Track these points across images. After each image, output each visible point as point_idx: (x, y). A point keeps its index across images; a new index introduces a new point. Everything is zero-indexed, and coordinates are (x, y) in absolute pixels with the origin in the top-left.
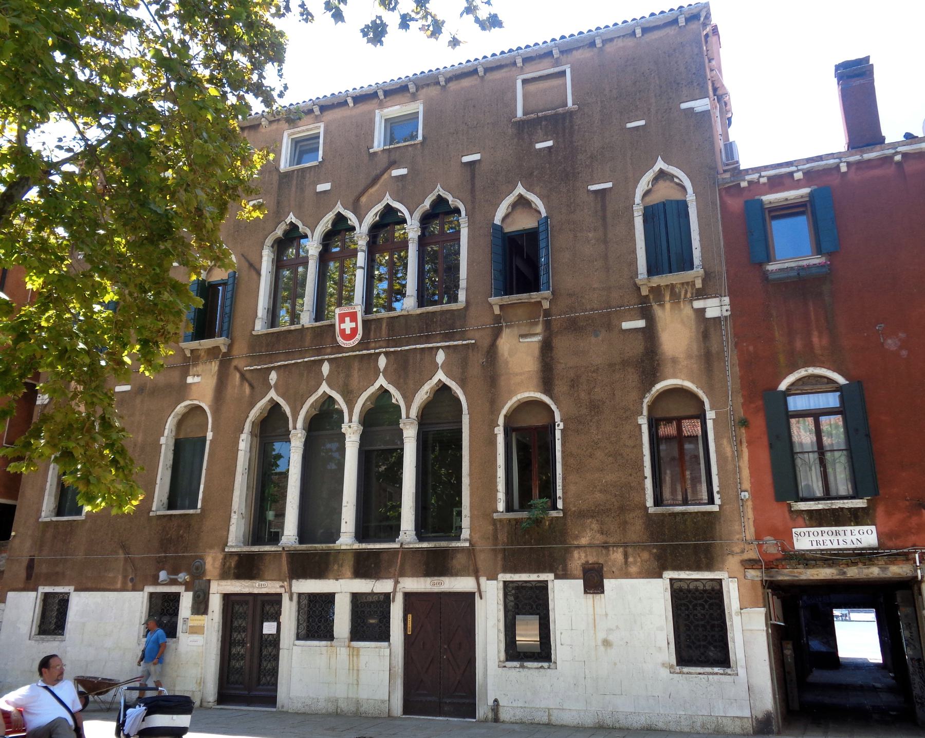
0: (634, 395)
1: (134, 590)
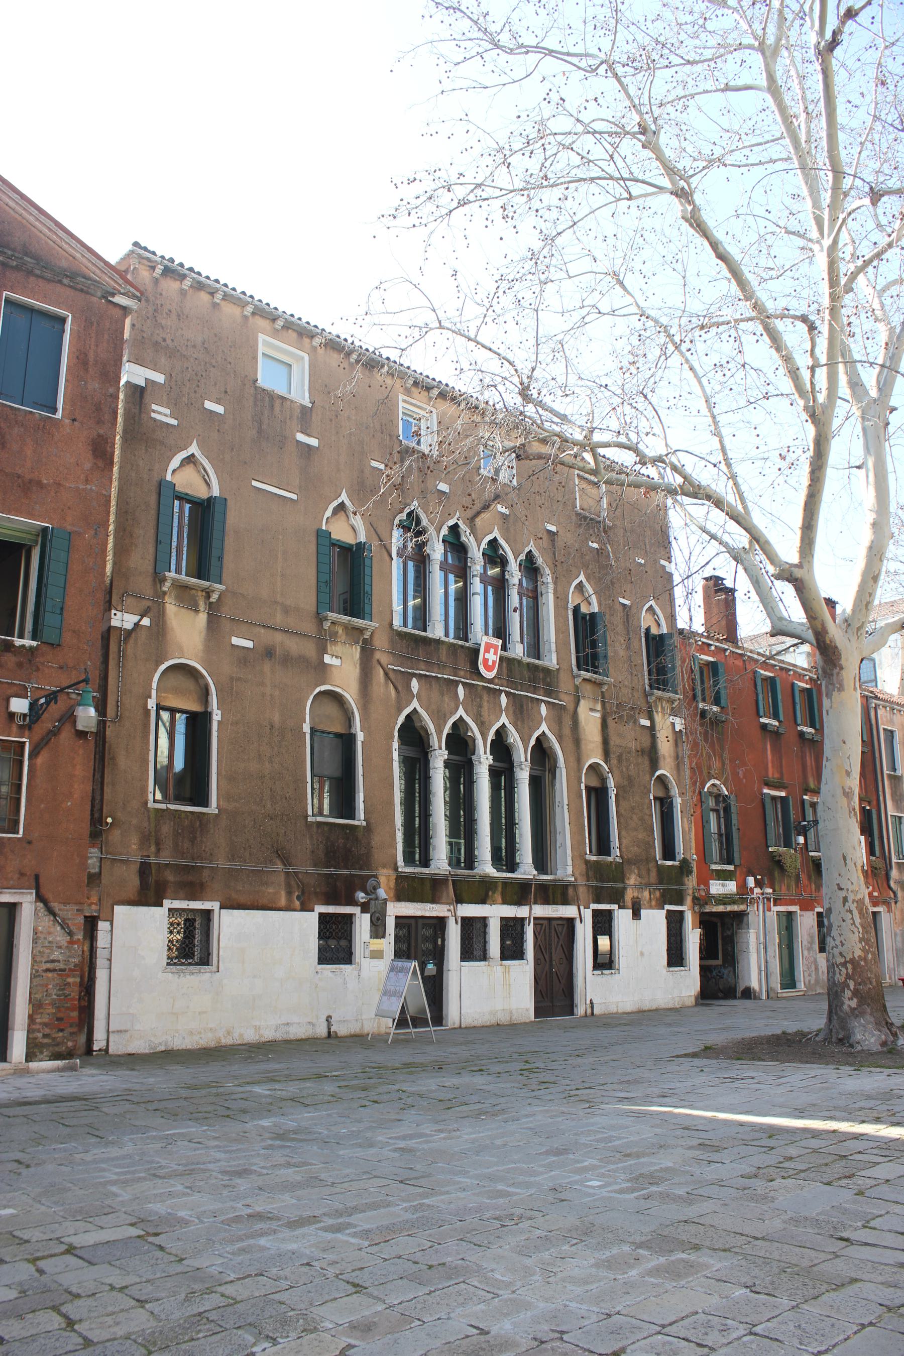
0: (647, 777)
1: (303, 909)
